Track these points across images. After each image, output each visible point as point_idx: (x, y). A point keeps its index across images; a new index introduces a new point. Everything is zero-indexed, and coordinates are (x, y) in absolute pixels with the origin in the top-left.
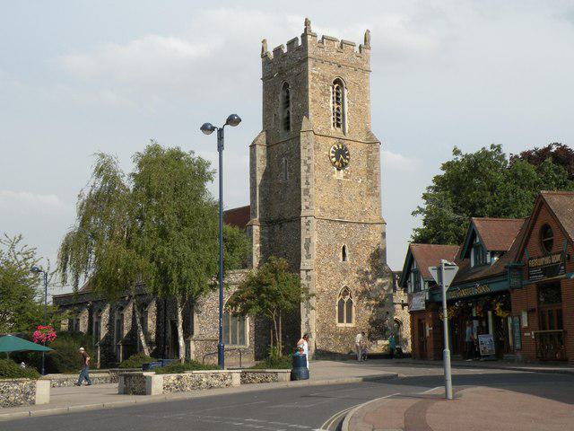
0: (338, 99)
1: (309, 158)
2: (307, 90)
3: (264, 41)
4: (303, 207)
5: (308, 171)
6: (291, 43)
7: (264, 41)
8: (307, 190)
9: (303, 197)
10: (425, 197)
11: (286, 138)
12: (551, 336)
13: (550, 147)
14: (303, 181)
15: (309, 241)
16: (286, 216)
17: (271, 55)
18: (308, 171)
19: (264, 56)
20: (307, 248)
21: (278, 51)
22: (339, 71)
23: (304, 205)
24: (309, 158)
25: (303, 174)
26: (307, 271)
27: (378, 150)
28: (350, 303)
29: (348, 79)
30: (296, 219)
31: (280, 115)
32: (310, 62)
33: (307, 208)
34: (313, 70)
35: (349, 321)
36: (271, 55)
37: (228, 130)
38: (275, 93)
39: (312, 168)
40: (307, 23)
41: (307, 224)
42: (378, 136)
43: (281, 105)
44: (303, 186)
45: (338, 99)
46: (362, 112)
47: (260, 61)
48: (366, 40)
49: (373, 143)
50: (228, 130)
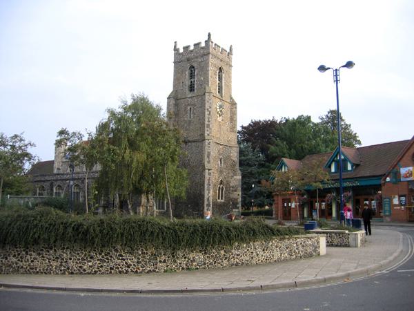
0: (220, 79)
1: (210, 107)
2: (209, 70)
3: (176, 42)
4: (206, 134)
5: (209, 114)
6: (197, 45)
7: (176, 42)
8: (208, 126)
9: (206, 129)
10: (356, 134)
11: (190, 95)
12: (204, 232)
13: (343, 120)
14: (207, 120)
15: (209, 153)
16: (190, 139)
17: (181, 51)
18: (209, 114)
19: (176, 49)
20: (208, 157)
21: (186, 48)
22: (221, 63)
23: (206, 133)
24: (210, 107)
25: (206, 116)
26: (209, 170)
27: (236, 108)
28: (223, 188)
29: (225, 68)
30: (203, 139)
31: (187, 82)
32: (210, 56)
33: (208, 135)
34: (211, 60)
35: (222, 199)
36: (181, 51)
37: (344, 72)
38: (183, 72)
39: (211, 113)
40: (209, 35)
41: (209, 144)
42: (236, 100)
43: (188, 77)
44: (206, 123)
45: (220, 79)
46: (229, 87)
47: (172, 53)
48: (231, 49)
49: (233, 104)
50: (344, 72)
